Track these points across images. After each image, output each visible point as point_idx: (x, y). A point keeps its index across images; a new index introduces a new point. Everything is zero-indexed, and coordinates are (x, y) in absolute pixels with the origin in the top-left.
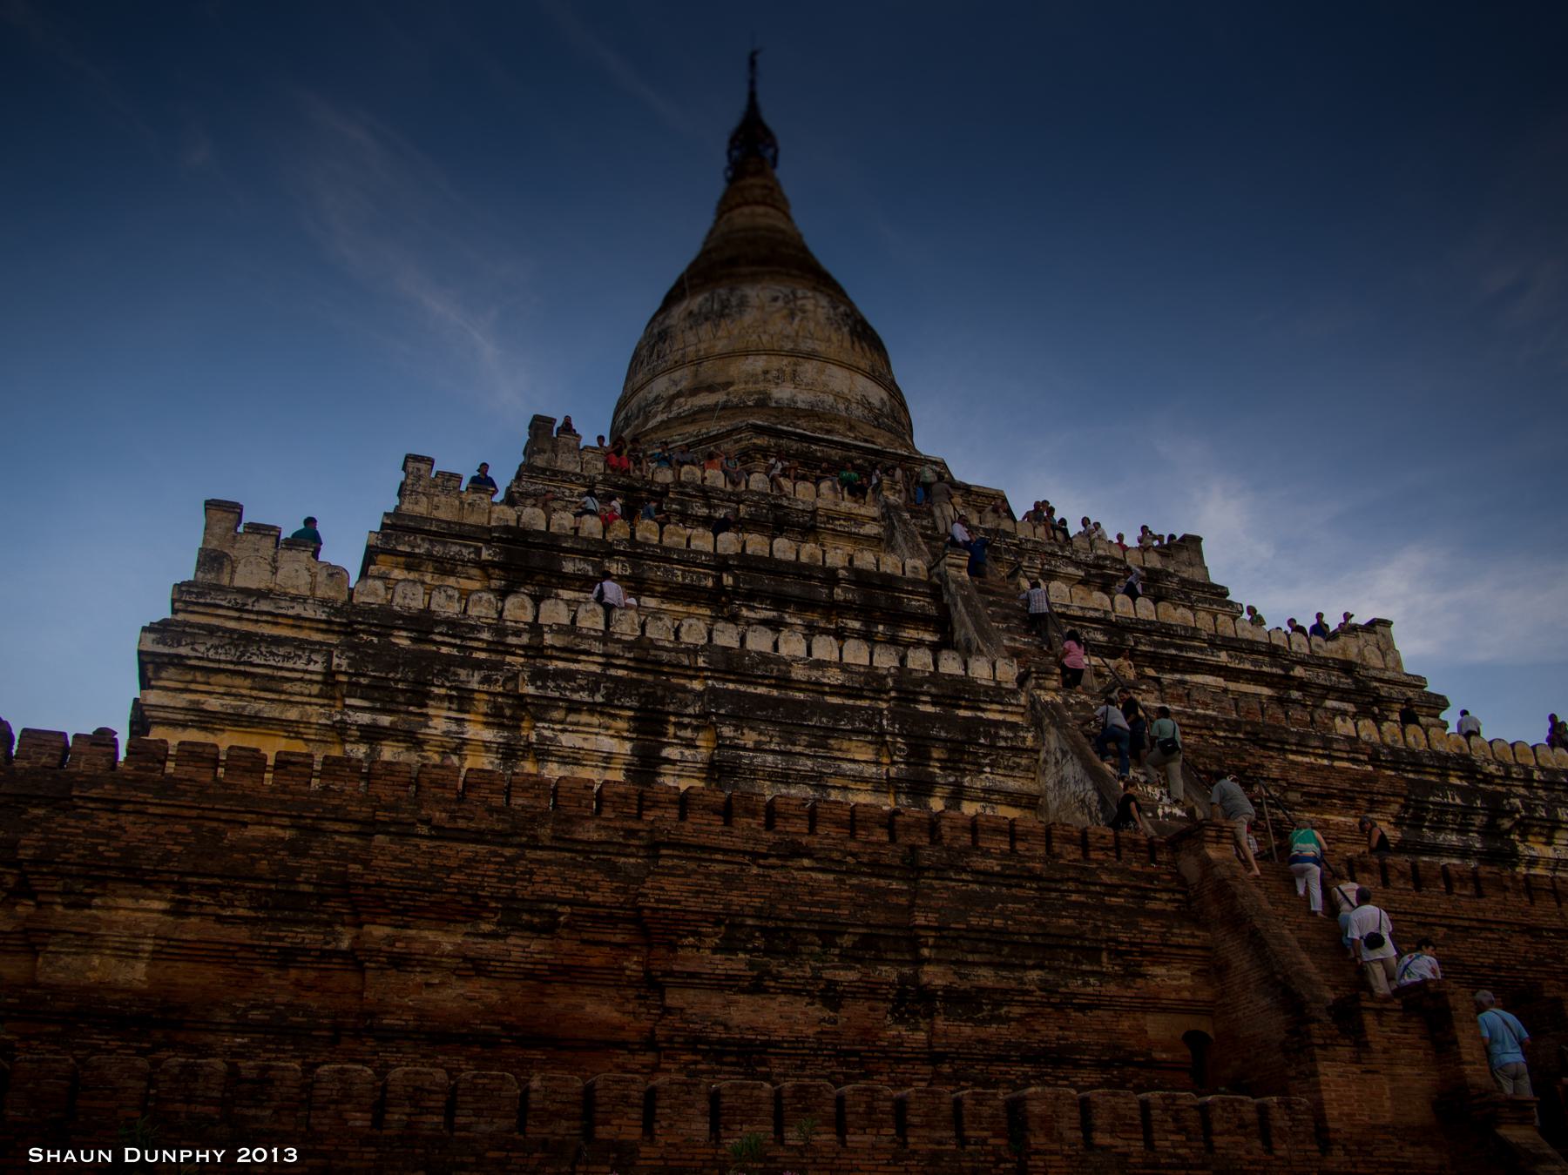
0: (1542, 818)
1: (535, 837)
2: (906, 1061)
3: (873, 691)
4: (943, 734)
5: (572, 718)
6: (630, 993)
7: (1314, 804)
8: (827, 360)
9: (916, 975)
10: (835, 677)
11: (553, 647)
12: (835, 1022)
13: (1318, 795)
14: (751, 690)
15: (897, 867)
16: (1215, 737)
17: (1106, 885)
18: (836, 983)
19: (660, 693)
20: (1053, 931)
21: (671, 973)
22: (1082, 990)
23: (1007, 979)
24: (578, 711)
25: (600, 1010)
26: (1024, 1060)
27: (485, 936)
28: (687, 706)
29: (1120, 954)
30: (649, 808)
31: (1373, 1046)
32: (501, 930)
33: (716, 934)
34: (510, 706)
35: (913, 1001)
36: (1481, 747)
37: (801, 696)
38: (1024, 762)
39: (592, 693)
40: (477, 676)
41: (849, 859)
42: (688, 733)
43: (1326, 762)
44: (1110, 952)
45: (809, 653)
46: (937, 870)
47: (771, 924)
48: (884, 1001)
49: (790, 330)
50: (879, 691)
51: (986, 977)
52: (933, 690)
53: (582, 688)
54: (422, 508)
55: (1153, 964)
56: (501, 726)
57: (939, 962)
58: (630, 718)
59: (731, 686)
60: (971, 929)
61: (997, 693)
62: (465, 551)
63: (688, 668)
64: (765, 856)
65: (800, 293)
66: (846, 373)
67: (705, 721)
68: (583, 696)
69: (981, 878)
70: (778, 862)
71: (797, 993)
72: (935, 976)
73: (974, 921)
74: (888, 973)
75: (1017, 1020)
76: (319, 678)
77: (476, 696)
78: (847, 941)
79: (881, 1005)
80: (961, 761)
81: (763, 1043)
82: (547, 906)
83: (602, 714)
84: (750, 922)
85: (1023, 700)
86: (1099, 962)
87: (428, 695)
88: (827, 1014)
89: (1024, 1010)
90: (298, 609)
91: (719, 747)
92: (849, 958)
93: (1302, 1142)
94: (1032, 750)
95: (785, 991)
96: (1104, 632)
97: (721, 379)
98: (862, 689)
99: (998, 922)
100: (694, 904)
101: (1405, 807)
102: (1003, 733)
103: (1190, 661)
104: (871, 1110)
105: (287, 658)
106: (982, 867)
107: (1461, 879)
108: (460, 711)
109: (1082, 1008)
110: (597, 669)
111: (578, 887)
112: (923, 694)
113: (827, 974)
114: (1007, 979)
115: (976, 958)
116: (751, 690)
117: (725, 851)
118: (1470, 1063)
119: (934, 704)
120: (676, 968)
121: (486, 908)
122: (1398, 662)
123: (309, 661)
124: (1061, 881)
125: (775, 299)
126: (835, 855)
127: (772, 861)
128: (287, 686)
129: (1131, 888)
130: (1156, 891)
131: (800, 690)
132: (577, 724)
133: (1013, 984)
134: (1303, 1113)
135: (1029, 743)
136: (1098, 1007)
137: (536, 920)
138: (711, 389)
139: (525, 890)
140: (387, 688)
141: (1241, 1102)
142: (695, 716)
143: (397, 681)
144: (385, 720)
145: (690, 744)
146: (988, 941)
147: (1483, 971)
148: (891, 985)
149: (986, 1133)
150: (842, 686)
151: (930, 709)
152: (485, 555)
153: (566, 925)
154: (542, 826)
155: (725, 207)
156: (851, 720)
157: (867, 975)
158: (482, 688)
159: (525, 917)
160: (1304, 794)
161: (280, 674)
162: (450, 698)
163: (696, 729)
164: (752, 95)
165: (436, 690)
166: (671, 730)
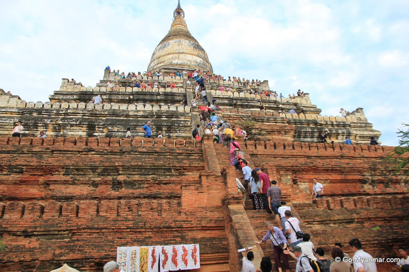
0: (334, 133)
1: (23, 151)
2: (112, 199)
3: (151, 116)
4: (165, 124)
5: (72, 128)
6: (42, 186)
7: (270, 134)
8: (186, 54)
9: (116, 178)
10: (141, 114)
11: (70, 113)
12: (95, 191)
13: (271, 131)
14: (119, 118)
15: (118, 152)
16: (243, 120)
17: (178, 153)
18: (95, 181)
19: (93, 121)
20: (156, 165)
21: (50, 181)
22: (164, 179)
23: (143, 178)
24: (73, 126)
25: (34, 191)
26: (145, 197)
27: (5, 175)
28: (100, 123)
29: (177, 170)
30: (56, 143)
31: (204, 185)
32: (9, 173)
33: (63, 171)
34: (58, 127)
35: (117, 185)
36: (321, 118)
37: (132, 119)
38: (188, 129)
39: (76, 122)
40: (49, 120)
41: (105, 151)
42: (101, 129)
43: (275, 124)
44: (174, 169)
45: (136, 109)
46: (128, 152)
47: (77, 168)
48: (110, 185)
49: (178, 48)
50: (153, 116)
51: (137, 177)
52: (166, 114)
53: (74, 121)
54: (64, 90)
55: (188, 172)
56: (56, 131)
57: (124, 174)
58: (86, 127)
59: (114, 118)
60: (131, 166)
61: (183, 114)
62: (71, 97)
63: (104, 115)
64: (82, 152)
65: (181, 40)
66: (191, 56)
67: (104, 126)
68: (74, 123)
69: (141, 153)
70: (86, 153)
71: (85, 184)
72: (121, 178)
73: (133, 164)
74: (110, 178)
75: (146, 188)
76: (13, 124)
77: (49, 125)
78: (99, 171)
79: (109, 186)
80: (171, 130)
81: (71, 197)
82: (19, 167)
83: (79, 126)
84: (71, 167)
85: (190, 115)
86: (171, 172)
87: (38, 126)
88: (94, 189)
89: (148, 185)
90: (11, 110)
91: (109, 131)
92: (99, 175)
93: (173, 213)
94: (189, 126)
95: (82, 184)
96: (228, 100)
97: (163, 61)
98: (148, 116)
99: (140, 164)
100: (56, 164)
101: (295, 133)
102: (182, 122)
103: (251, 105)
104: (33, 208)
105: (5, 120)
106: (141, 151)
107: (288, 145)
108: (46, 129)
109: (165, 184)
110: (81, 117)
111: (28, 162)
112: (163, 115)
113: (92, 179)
114: (143, 178)
115: (135, 173)
116: (119, 118)
117: (71, 151)
118: (231, 188)
119: (166, 118)
120: (51, 179)
121: (4, 168)
122: (310, 103)
123: (10, 120)
124: (165, 153)
125: (176, 42)
126: (101, 150)
127: (84, 153)
128: (6, 127)
129: (186, 153)
130: (193, 154)
131: (132, 117)
132: (73, 129)
133: (144, 179)
134: (174, 205)
135: (189, 124)
136: (170, 183)
137: (17, 170)
138: (161, 63)
139: (13, 163)
140: (28, 125)
141: (153, 202)
142: (102, 125)
143: (30, 123)
144: (27, 132)
145: (102, 132)
146: (137, 168)
147: (288, 168)
148: (110, 181)
149: (69, 214)
150: (143, 115)
151: (165, 119)
152: (75, 97)
153: (26, 171)
154: (25, 148)
155: (173, 26)
156: (142, 123)
157: (104, 179)
158: (51, 123)
159: (15, 170)
160: (266, 131)
161: (3, 124)
162: (43, 126)
163: (103, 128)
164: (179, 3)
165: (39, 125)
166: (97, 129)
